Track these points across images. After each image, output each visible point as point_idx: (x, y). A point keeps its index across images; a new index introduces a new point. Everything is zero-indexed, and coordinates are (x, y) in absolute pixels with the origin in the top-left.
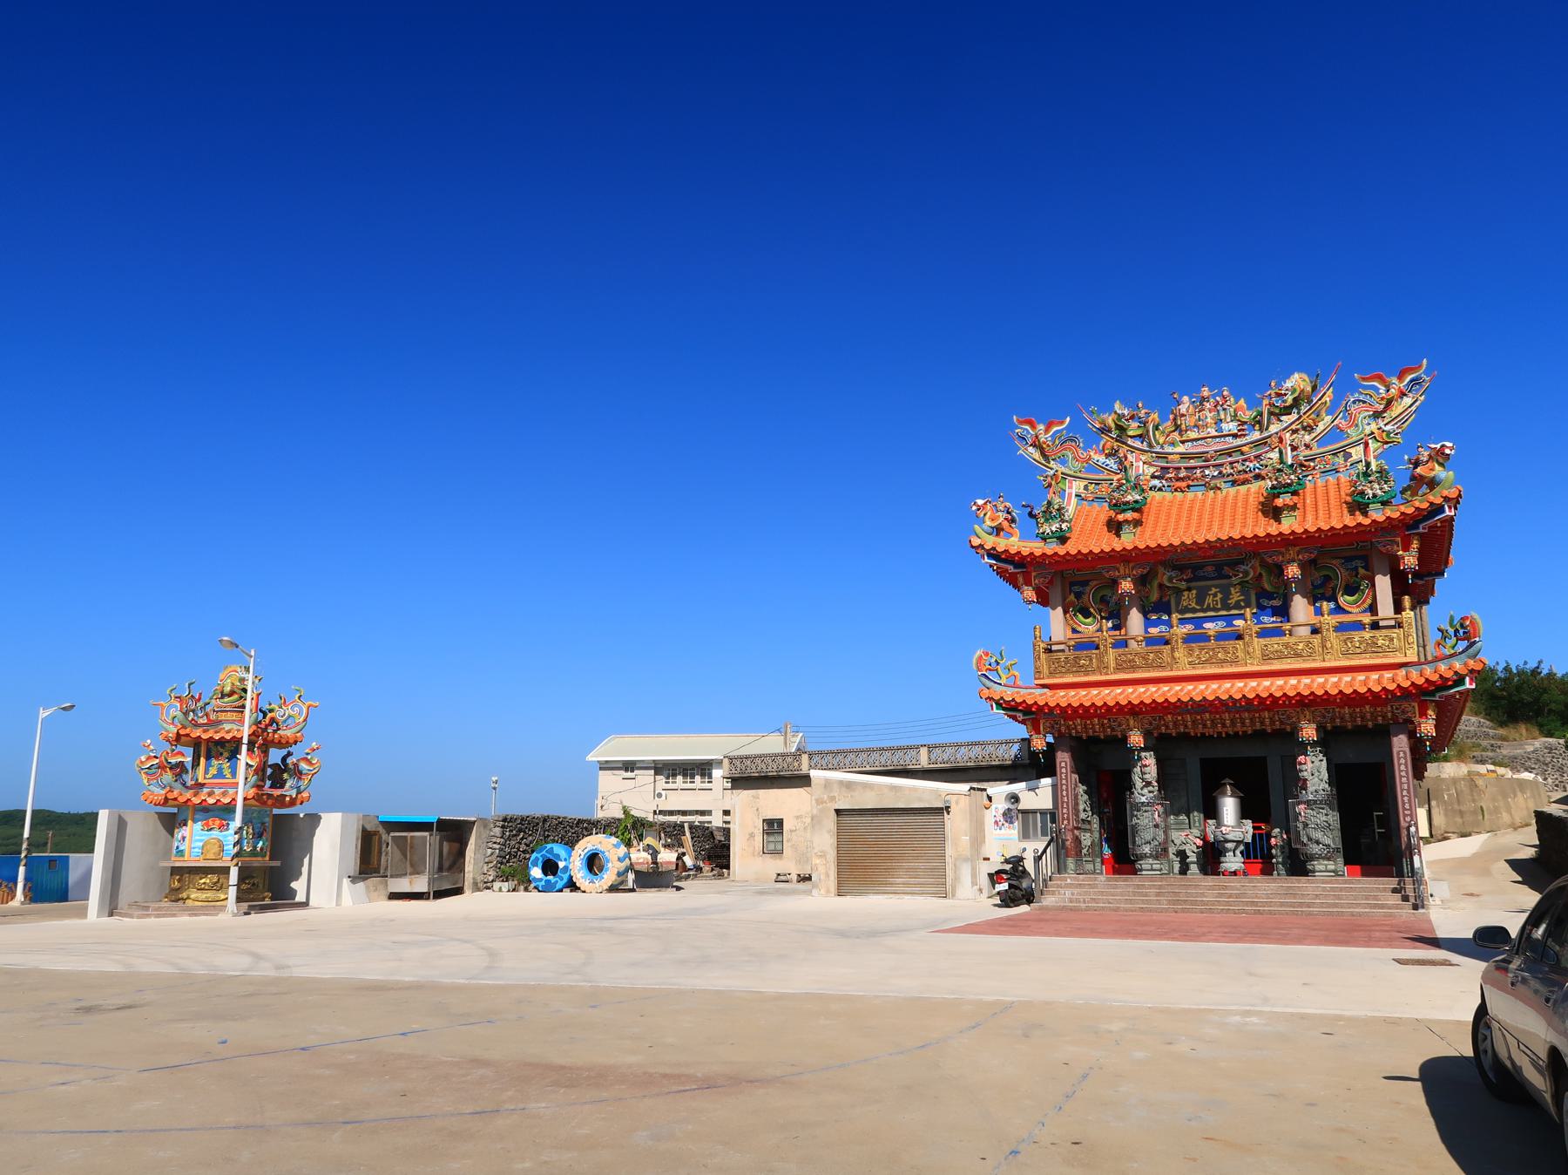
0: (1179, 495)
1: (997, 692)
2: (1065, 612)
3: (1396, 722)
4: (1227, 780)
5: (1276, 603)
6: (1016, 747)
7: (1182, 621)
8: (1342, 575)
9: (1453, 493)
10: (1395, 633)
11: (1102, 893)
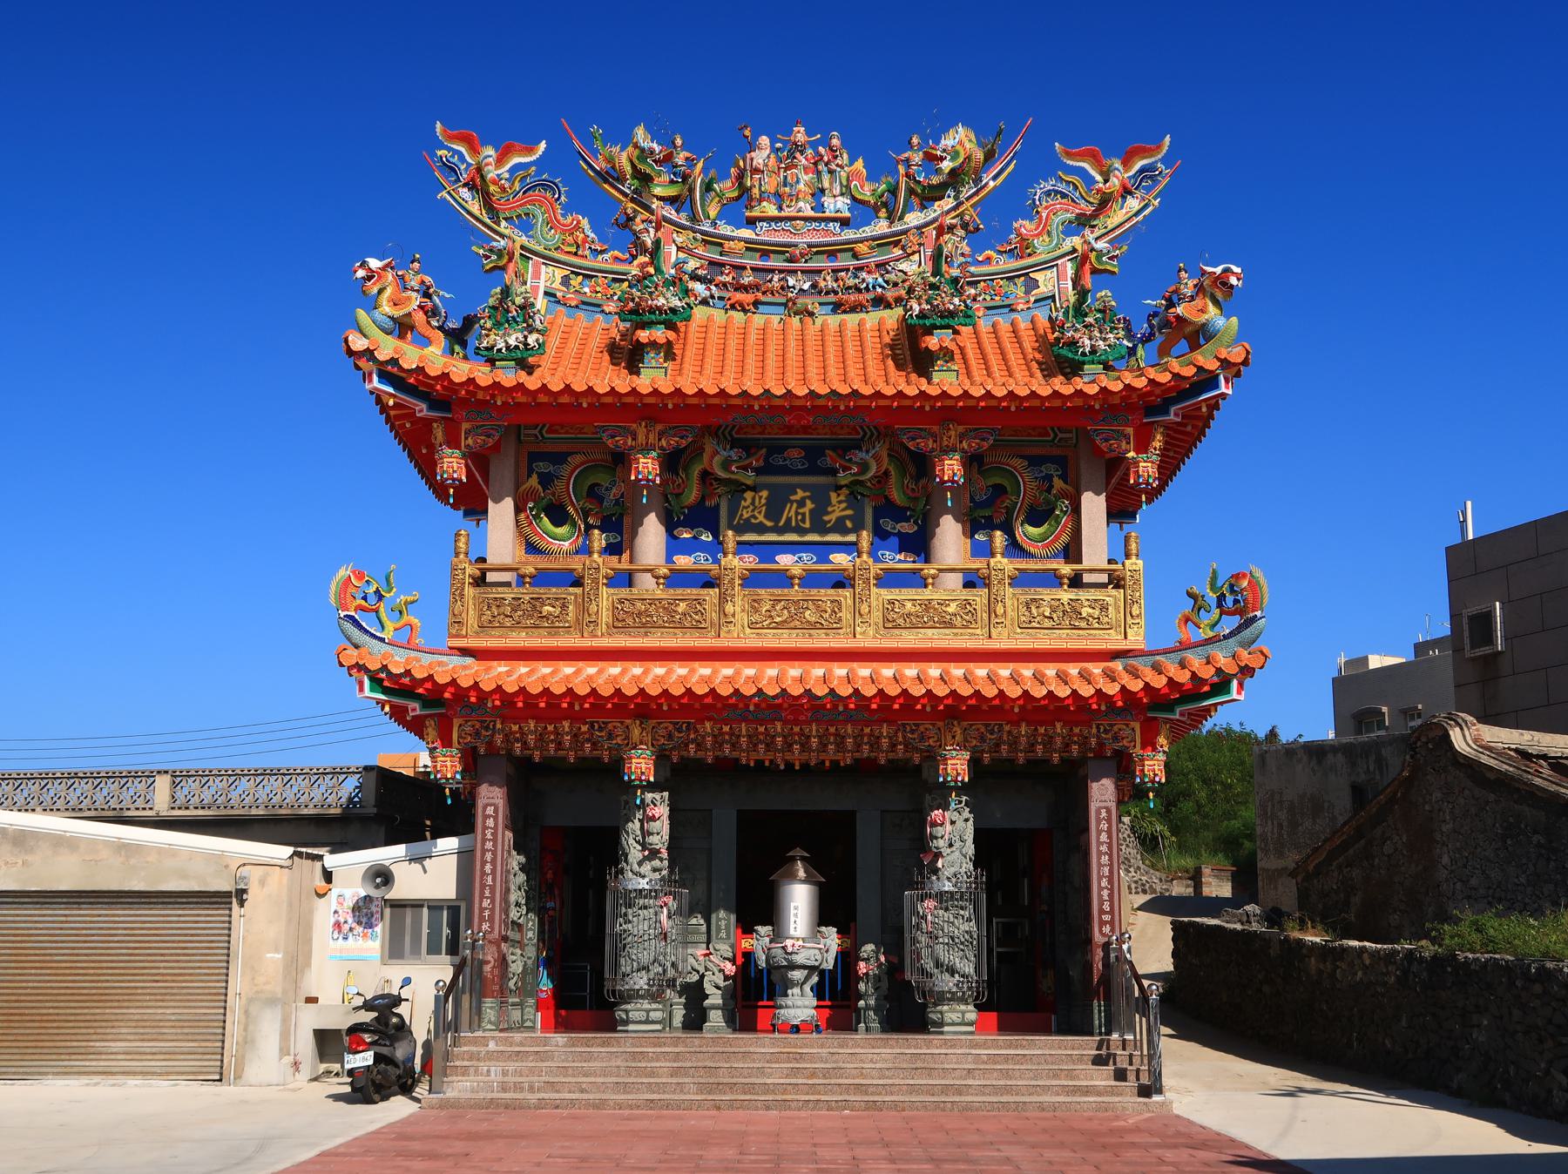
0: (738, 316)
1: (374, 654)
2: (518, 510)
3: (1099, 754)
4: (798, 852)
5: (907, 528)
6: (352, 783)
7: (743, 547)
8: (1027, 486)
9: (1236, 354)
10: (1112, 596)
11: (564, 1070)
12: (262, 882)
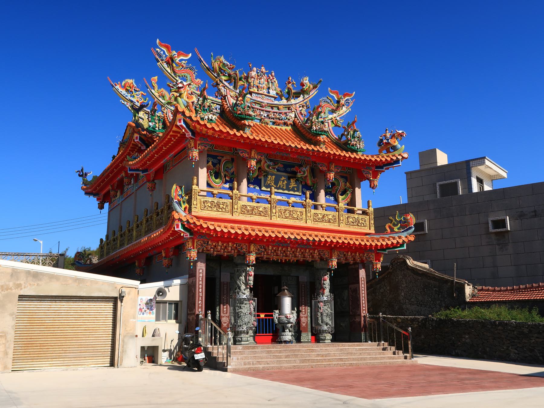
12: (129, 294)
